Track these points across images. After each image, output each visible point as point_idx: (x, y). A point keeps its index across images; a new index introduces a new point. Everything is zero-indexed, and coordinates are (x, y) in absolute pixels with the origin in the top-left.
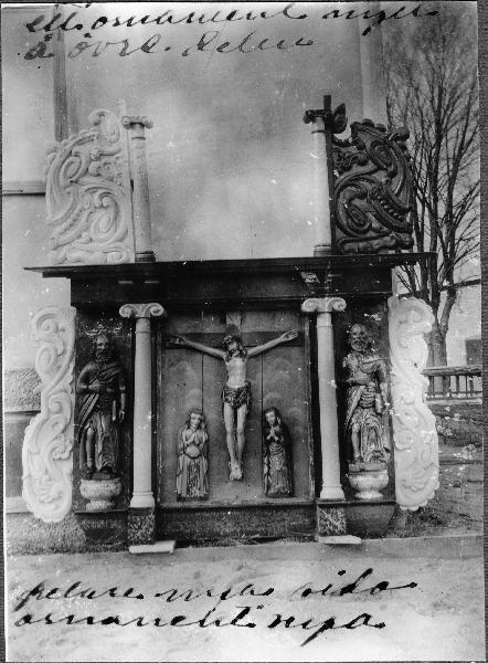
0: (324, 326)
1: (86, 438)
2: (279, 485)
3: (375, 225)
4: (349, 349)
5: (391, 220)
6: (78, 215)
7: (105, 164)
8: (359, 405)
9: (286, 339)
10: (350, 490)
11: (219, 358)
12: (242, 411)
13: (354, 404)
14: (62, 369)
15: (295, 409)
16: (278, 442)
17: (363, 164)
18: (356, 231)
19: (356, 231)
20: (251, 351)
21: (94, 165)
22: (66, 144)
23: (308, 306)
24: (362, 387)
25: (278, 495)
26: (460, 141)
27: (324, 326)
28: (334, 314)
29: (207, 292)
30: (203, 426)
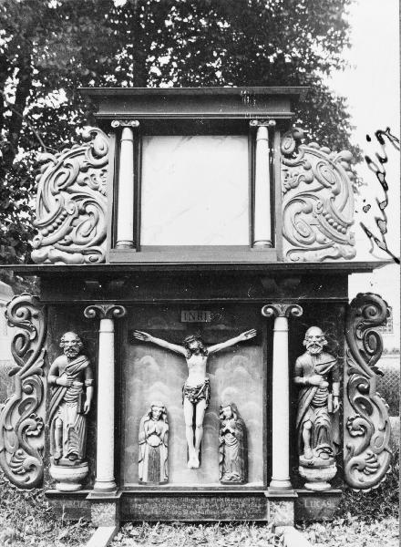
0: (281, 325)
1: (54, 427)
2: (233, 473)
3: (321, 236)
4: (303, 350)
5: (335, 232)
6: (63, 220)
7: (92, 175)
8: (311, 404)
9: (244, 338)
10: (297, 480)
11: (180, 356)
12: (202, 405)
13: (307, 403)
14: (33, 355)
15: (251, 403)
16: (233, 434)
17: (309, 182)
18: (302, 242)
19: (302, 242)
20: (211, 349)
21: (82, 176)
22: (58, 157)
23: (267, 311)
24: (314, 389)
25: (232, 481)
26: (87, 403)
27: (281, 325)
28: (291, 319)
29: (266, 283)
30: (164, 416)
